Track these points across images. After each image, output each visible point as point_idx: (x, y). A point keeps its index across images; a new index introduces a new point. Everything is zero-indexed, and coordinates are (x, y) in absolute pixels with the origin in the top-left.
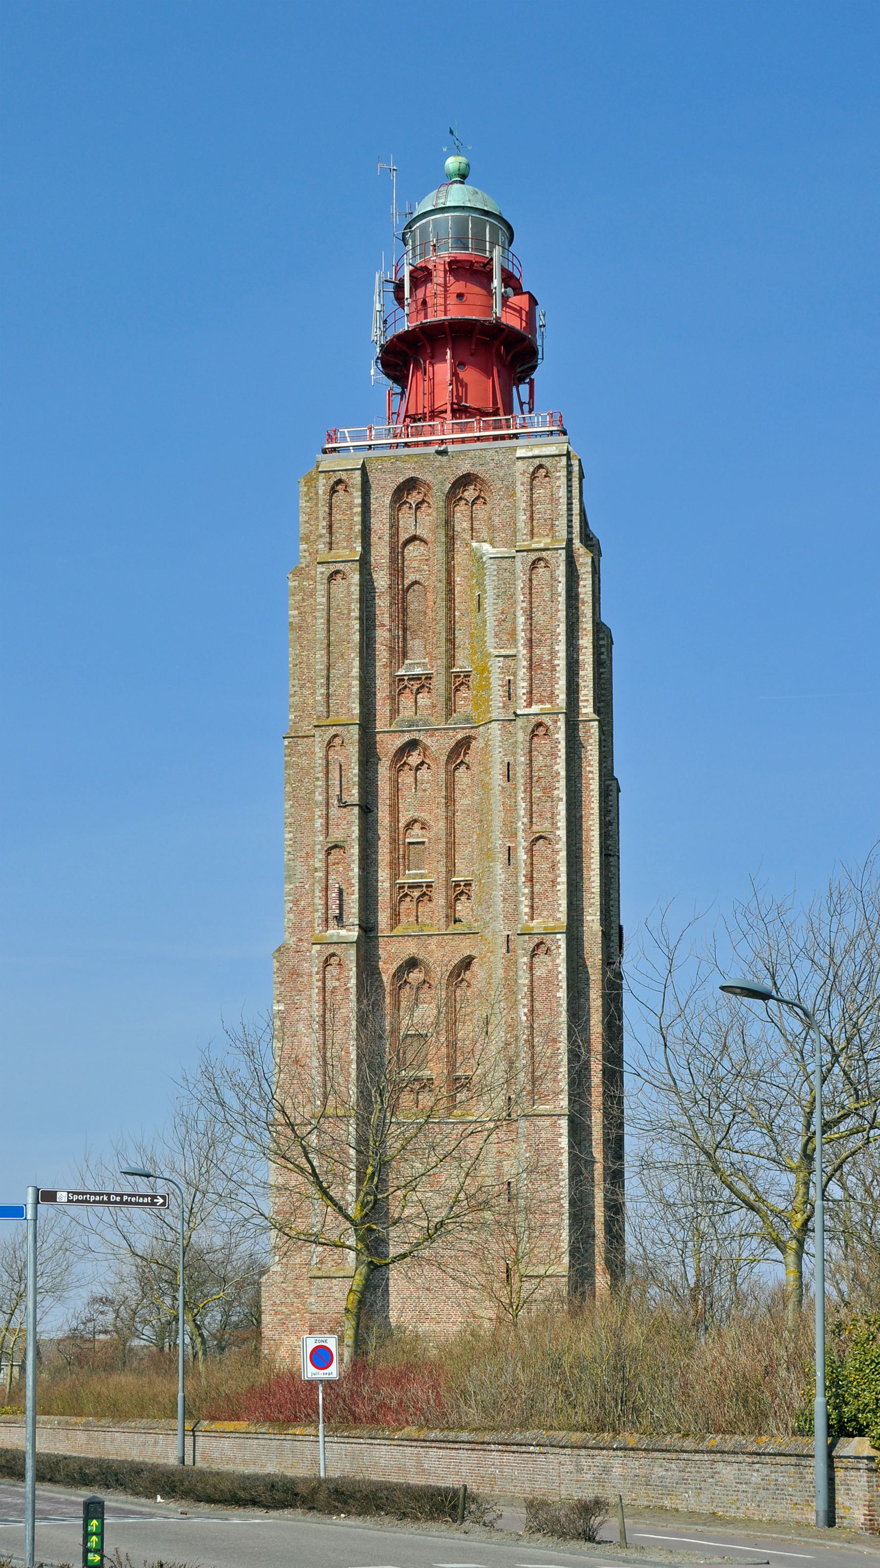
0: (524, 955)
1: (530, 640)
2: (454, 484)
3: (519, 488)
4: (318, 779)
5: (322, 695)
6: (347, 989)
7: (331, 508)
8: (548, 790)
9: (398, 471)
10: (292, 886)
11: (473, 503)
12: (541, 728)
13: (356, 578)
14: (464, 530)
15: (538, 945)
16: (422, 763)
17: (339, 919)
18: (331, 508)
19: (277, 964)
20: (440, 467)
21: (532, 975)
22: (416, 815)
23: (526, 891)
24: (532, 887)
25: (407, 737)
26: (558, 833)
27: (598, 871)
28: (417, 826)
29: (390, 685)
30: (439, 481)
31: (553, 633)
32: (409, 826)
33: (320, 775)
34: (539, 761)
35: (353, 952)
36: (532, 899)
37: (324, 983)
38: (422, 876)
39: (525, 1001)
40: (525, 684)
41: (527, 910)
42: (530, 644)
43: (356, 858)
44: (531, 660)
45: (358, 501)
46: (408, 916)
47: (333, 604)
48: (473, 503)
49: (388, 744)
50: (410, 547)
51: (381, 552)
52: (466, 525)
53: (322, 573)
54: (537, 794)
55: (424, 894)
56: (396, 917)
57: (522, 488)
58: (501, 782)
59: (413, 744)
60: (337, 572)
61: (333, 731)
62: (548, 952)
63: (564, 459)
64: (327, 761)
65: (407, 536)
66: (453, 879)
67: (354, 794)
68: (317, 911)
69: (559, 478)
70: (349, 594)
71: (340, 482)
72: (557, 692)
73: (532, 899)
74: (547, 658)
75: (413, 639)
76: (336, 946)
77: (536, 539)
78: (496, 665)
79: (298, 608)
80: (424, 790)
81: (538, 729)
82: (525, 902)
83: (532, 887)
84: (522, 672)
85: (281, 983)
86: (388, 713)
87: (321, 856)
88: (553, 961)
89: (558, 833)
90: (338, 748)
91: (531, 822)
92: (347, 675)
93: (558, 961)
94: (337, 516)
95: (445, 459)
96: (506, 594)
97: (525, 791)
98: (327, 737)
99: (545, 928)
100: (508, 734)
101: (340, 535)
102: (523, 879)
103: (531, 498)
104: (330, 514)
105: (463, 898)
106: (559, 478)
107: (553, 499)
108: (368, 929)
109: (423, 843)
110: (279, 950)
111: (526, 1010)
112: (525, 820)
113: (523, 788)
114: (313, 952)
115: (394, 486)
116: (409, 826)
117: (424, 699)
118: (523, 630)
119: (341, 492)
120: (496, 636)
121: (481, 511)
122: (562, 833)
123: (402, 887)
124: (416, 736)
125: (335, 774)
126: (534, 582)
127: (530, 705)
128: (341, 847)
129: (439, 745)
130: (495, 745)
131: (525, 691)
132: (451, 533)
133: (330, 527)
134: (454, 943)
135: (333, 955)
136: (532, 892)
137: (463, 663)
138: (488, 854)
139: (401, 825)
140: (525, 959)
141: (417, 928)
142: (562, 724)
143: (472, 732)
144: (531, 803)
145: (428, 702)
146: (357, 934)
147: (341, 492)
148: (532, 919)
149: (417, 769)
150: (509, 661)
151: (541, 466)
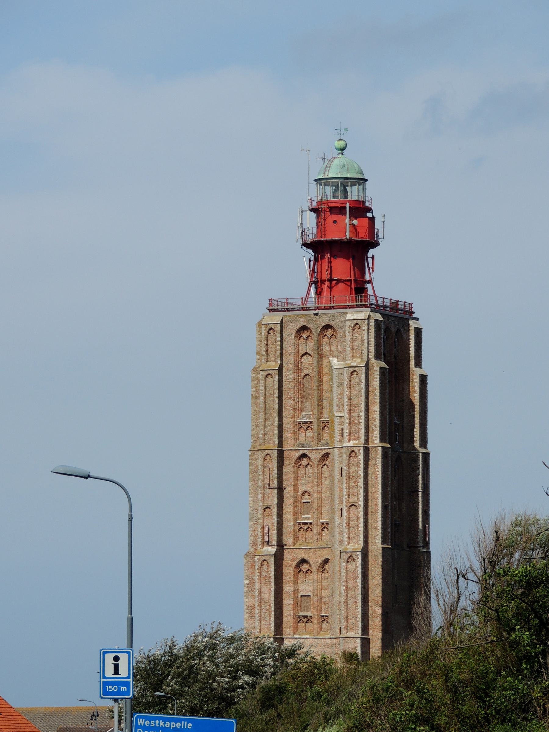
0: (344, 562)
1: (350, 410)
2: (321, 330)
3: (348, 334)
4: (260, 475)
5: (262, 434)
6: (270, 577)
7: (267, 341)
8: (356, 482)
9: (297, 322)
10: (252, 523)
11: (331, 337)
12: (354, 453)
13: (276, 378)
14: (327, 350)
15: (349, 557)
16: (308, 464)
17: (268, 543)
18: (267, 341)
19: (246, 561)
20: (315, 321)
21: (347, 571)
22: (306, 489)
23: (346, 530)
24: (349, 529)
25: (301, 453)
26: (360, 503)
27: (380, 519)
28: (306, 494)
29: (294, 427)
30: (316, 328)
31: (360, 408)
32: (303, 494)
33: (261, 473)
34: (353, 468)
35: (273, 559)
36: (349, 534)
37: (261, 574)
38: (308, 519)
39: (344, 584)
40: (347, 431)
41: (347, 540)
42: (350, 411)
43: (275, 513)
44: (350, 419)
45: (279, 339)
46: (302, 538)
47: (268, 390)
48: (331, 337)
49: (291, 455)
50: (305, 357)
51: (289, 363)
52: (328, 348)
53: (262, 375)
54: (352, 484)
55: (309, 527)
56: (296, 538)
57: (349, 334)
58: (338, 477)
59: (304, 456)
60: (269, 374)
61: (266, 452)
62: (354, 560)
63: (367, 321)
64: (264, 467)
65: (303, 353)
66: (321, 521)
67: (275, 483)
68: (259, 538)
69: (364, 330)
70: (274, 385)
71: (271, 329)
72: (360, 435)
73: (349, 534)
74: (357, 418)
75: (306, 402)
76: (265, 556)
77: (355, 359)
78: (337, 420)
79: (255, 387)
80: (310, 477)
81: (352, 453)
82: (346, 536)
83: (349, 529)
84: (346, 425)
85: (247, 570)
86: (293, 440)
87: (261, 512)
88: (356, 564)
89: (360, 503)
90: (268, 460)
91: (349, 497)
92: (273, 424)
93: (358, 565)
94: (270, 345)
95: (317, 317)
96: (341, 386)
97: (346, 483)
98: (264, 455)
99: (353, 549)
100: (341, 453)
101: (271, 355)
102: (345, 525)
103: (353, 339)
104: (267, 345)
105: (326, 529)
106: (364, 330)
107: (362, 341)
108: (281, 546)
109: (309, 502)
110: (246, 554)
111: (344, 588)
112: (346, 497)
113: (345, 481)
114: (256, 559)
115: (296, 329)
116: (303, 494)
117: (309, 433)
118: (347, 405)
119: (272, 334)
120: (337, 406)
121: (334, 341)
122: (361, 503)
123: (299, 524)
124: (305, 452)
125: (267, 473)
126: (352, 382)
127: (349, 441)
128: (270, 508)
129: (315, 456)
130: (338, 459)
131: (347, 434)
132: (321, 353)
133: (267, 351)
134: (320, 552)
135: (265, 560)
136: (349, 531)
137: (326, 417)
138: (333, 511)
139: (300, 493)
140: (344, 564)
141: (305, 544)
142: (362, 451)
143: (328, 451)
144: (349, 488)
145: (311, 434)
146: (275, 550)
147: (272, 334)
148: (349, 544)
149: (306, 466)
150: (342, 419)
151: (357, 324)
